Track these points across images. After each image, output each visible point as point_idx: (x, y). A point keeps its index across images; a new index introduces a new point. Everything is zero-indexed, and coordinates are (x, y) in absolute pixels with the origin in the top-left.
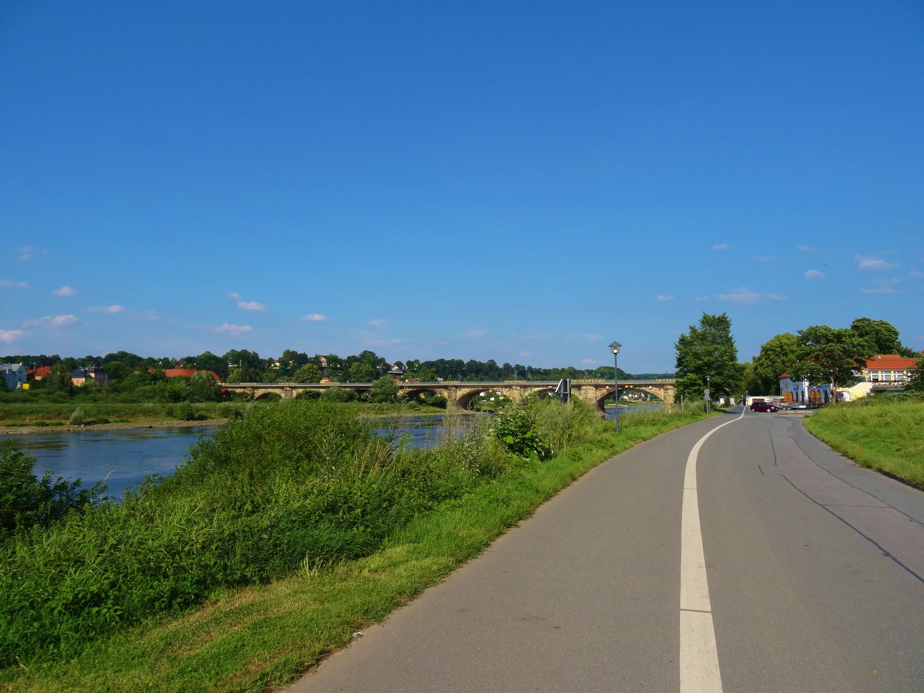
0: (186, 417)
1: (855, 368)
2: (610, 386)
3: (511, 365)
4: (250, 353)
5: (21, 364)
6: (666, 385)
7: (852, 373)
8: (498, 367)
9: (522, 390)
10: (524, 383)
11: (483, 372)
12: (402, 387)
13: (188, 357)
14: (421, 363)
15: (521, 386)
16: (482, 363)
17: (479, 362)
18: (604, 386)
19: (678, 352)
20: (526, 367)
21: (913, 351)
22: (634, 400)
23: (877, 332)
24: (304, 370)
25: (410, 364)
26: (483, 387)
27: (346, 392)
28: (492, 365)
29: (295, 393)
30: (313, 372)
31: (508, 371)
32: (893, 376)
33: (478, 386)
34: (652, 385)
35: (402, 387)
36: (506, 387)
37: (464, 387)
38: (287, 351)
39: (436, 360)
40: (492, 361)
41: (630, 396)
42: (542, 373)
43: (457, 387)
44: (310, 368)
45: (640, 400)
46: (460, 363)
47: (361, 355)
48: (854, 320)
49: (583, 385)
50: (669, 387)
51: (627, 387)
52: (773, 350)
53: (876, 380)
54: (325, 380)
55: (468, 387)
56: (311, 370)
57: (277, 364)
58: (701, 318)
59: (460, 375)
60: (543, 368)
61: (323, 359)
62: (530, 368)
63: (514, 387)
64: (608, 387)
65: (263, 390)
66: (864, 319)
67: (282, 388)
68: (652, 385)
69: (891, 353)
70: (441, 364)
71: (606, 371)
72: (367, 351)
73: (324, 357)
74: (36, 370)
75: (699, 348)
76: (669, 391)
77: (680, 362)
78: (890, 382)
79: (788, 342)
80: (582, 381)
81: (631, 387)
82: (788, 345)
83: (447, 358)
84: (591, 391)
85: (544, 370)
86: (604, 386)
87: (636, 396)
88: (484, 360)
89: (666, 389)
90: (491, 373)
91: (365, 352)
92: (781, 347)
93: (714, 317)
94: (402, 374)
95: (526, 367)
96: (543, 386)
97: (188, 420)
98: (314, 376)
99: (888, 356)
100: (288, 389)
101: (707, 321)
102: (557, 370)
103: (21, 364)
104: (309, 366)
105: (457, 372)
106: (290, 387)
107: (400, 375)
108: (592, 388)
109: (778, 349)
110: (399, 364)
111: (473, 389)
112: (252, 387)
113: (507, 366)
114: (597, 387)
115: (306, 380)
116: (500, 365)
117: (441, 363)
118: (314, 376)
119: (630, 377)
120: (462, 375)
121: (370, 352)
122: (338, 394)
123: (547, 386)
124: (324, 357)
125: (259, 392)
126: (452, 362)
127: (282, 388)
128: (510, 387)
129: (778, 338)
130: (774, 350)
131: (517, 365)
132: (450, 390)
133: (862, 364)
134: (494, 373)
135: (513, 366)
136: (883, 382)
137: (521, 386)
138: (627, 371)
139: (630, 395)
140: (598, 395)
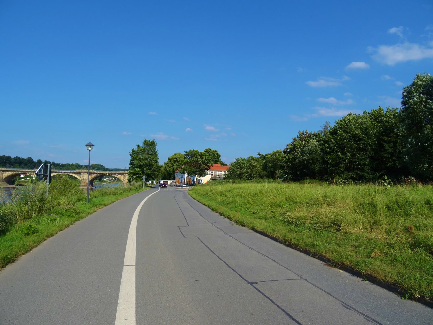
2: (96, 173)
6: (125, 174)
16: (23, 159)
17: (22, 158)
18: (93, 173)
19: (131, 157)
22: (109, 181)
23: (213, 154)
33: (18, 171)
37: (9, 171)
40: (30, 158)
42: (60, 166)
43: (3, 171)
45: (112, 181)
46: (9, 158)
49: (82, 173)
50: (126, 175)
51: (105, 174)
53: (212, 175)
55: (11, 171)
60: (61, 163)
64: (95, 174)
66: (209, 149)
69: (217, 164)
75: (141, 156)
76: (126, 177)
78: (217, 175)
79: (179, 156)
80: (81, 171)
81: (108, 174)
82: (179, 158)
84: (86, 176)
85: (62, 164)
86: (93, 173)
87: (110, 179)
89: (125, 176)
92: (177, 159)
96: (59, 172)
99: (216, 165)
105: (6, 163)
108: (87, 174)
109: (175, 160)
129: (175, 154)
130: (173, 160)
133: (209, 168)
134: (31, 164)
136: (214, 175)
138: (106, 167)
139: (107, 178)
140: (90, 178)
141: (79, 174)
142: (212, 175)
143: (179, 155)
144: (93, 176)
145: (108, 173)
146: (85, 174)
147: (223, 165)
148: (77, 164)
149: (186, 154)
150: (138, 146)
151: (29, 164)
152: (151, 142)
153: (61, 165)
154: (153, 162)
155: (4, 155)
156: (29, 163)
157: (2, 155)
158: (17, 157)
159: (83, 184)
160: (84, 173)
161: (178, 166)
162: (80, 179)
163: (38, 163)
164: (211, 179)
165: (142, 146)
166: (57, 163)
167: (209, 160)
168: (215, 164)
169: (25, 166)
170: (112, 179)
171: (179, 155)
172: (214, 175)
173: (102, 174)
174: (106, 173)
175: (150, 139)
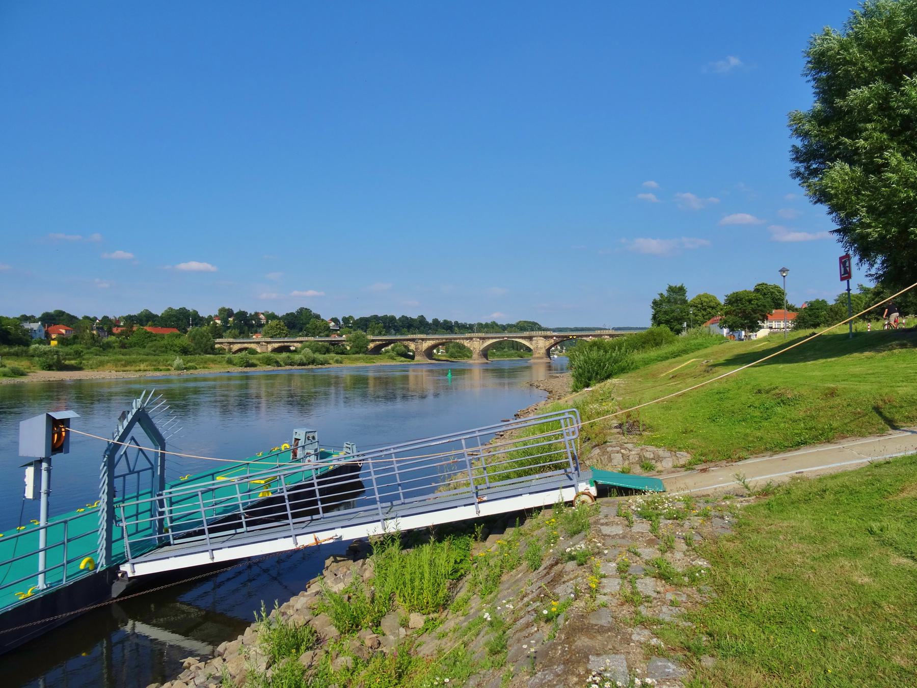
0: (245, 364)
1: (760, 320)
2: (557, 337)
5: (40, 323)
6: (604, 335)
7: (758, 323)
10: (482, 335)
12: (373, 341)
15: (480, 338)
16: (413, 319)
18: (552, 337)
19: (653, 311)
20: (453, 322)
21: (796, 307)
23: (772, 293)
25: (346, 320)
27: (323, 346)
28: (422, 320)
29: (270, 347)
30: (280, 328)
31: (437, 326)
32: (782, 325)
35: (373, 341)
36: (467, 339)
37: (429, 339)
39: (140, 312)
40: (422, 316)
42: (467, 328)
43: (423, 340)
44: (277, 325)
46: (392, 319)
47: (298, 312)
48: (756, 285)
49: (535, 337)
51: (571, 337)
52: (695, 306)
53: (771, 328)
55: (433, 339)
57: (218, 322)
58: (667, 288)
60: (468, 323)
61: (262, 316)
62: (456, 323)
64: (555, 338)
66: (763, 284)
67: (258, 343)
69: (781, 308)
71: (525, 325)
73: (263, 314)
74: (48, 328)
75: (665, 307)
77: (654, 318)
78: (780, 329)
79: (706, 300)
80: (533, 333)
81: (575, 337)
82: (707, 302)
84: (541, 341)
85: (469, 325)
86: (552, 337)
88: (415, 316)
91: (302, 309)
92: (702, 304)
93: (676, 287)
94: (338, 330)
95: (453, 322)
96: (499, 338)
97: (246, 367)
99: (779, 311)
100: (264, 344)
101: (671, 289)
102: (482, 324)
103: (40, 323)
105: (390, 327)
106: (265, 342)
107: (337, 330)
108: (542, 338)
109: (700, 306)
110: (335, 320)
111: (437, 341)
112: (228, 343)
114: (546, 337)
116: (430, 320)
117: (375, 318)
121: (306, 309)
122: (317, 348)
123: (503, 337)
124: (263, 314)
125: (236, 347)
126: (385, 317)
127: (258, 343)
128: (471, 339)
129: (699, 297)
130: (696, 306)
131: (445, 321)
133: (764, 318)
135: (442, 322)
136: (775, 329)
137: (480, 338)
138: (543, 325)
141: (530, 338)
142: (771, 328)
144: (552, 341)
146: (539, 338)
147: (793, 311)
148: (494, 322)
149: (726, 298)
150: (661, 295)
151: (422, 328)
152: (679, 287)
154: (684, 314)
155: (166, 308)
159: (537, 355)
160: (537, 336)
161: (705, 317)
162: (532, 347)
164: (770, 332)
165: (666, 294)
167: (765, 306)
168: (776, 309)
172: (775, 329)
173: (566, 337)
174: (573, 336)
175: (677, 284)
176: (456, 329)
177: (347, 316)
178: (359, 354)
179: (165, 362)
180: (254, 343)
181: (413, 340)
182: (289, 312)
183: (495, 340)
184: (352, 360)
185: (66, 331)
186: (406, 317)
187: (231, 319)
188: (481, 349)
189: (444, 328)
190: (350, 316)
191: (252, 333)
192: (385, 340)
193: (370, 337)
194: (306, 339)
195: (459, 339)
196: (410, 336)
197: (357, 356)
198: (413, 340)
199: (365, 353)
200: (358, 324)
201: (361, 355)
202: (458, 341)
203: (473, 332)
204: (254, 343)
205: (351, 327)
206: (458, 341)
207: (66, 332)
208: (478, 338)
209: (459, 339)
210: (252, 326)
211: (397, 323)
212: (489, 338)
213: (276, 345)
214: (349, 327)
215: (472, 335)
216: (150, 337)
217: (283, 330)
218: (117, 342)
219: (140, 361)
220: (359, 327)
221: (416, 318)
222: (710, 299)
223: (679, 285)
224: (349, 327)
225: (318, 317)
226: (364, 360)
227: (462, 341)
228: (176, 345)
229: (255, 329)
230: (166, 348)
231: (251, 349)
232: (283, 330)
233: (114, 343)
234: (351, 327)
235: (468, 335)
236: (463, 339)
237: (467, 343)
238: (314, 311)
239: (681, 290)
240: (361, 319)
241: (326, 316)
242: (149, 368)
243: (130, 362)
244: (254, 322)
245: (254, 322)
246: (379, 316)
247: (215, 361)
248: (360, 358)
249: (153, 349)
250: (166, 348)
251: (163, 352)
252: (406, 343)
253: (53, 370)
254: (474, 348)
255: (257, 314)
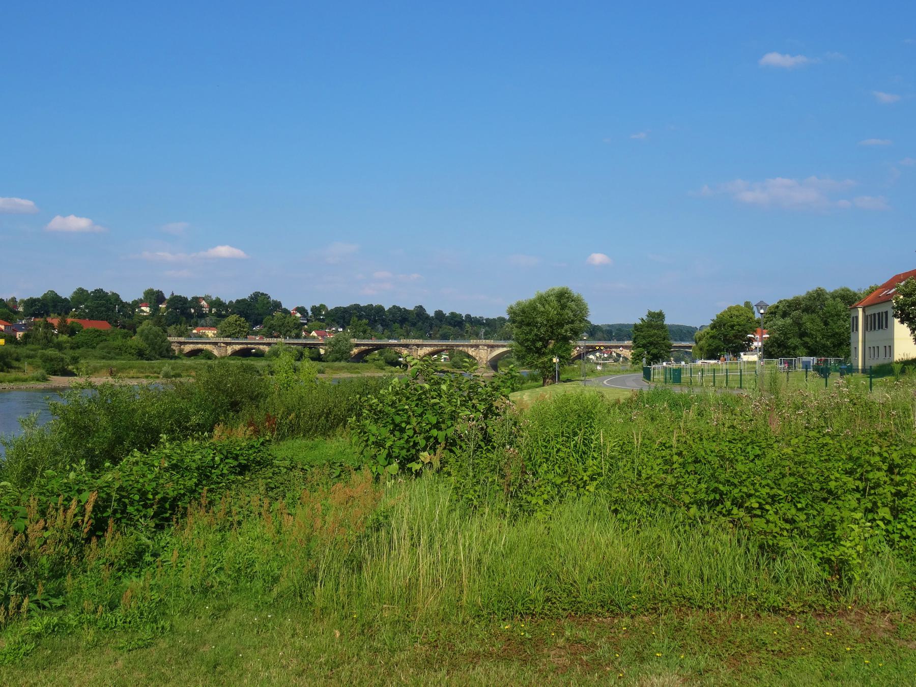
3: (444, 313)
4: (107, 293)
8: (428, 316)
9: (489, 350)
10: (491, 342)
11: (408, 321)
13: (31, 298)
14: (329, 309)
15: (489, 346)
16: (407, 310)
17: (404, 309)
24: (229, 323)
25: (317, 310)
26: (447, 346)
29: (230, 350)
30: (240, 324)
31: (441, 321)
33: (442, 345)
34: (622, 346)
35: (357, 345)
36: (472, 346)
37: (426, 346)
38: (149, 290)
40: (421, 307)
41: (598, 356)
42: (483, 324)
43: (418, 346)
44: (236, 321)
45: (611, 361)
46: (380, 309)
47: (251, 298)
51: (597, 348)
54: (213, 332)
55: (430, 346)
56: (238, 322)
58: (647, 313)
59: (379, 326)
60: (485, 317)
61: (204, 303)
62: (468, 316)
63: (481, 347)
65: (191, 345)
68: (622, 346)
70: (355, 311)
72: (259, 293)
79: (736, 313)
83: (363, 304)
85: (487, 320)
87: (606, 355)
90: (420, 323)
98: (242, 329)
100: (222, 345)
101: (651, 315)
104: (235, 318)
105: (376, 321)
106: (224, 343)
110: (301, 310)
113: (439, 314)
115: (233, 334)
116: (431, 312)
117: (355, 309)
118: (242, 329)
119: (598, 329)
120: (382, 326)
121: (262, 294)
124: (204, 299)
126: (370, 308)
128: (477, 346)
129: (730, 309)
131: (452, 313)
132: (411, 349)
134: (423, 323)
135: (448, 315)
137: (489, 346)
143: (738, 311)
145: (603, 346)
153: (484, 321)
156: (419, 321)
157: (366, 305)
158: (394, 306)
163: (436, 318)
165: (645, 318)
166: (476, 317)
169: (412, 328)
170: (610, 356)
171: (738, 311)
176: (468, 325)
177: (317, 305)
178: (340, 361)
179: (151, 369)
180: (209, 343)
181: (406, 346)
182: (240, 298)
183: (505, 349)
184: (335, 370)
185: (6, 326)
186: (399, 308)
187: (162, 306)
188: (489, 358)
189: (450, 324)
190: (321, 305)
191: (190, 326)
192: (371, 345)
193: (355, 341)
194: (275, 340)
195: (463, 346)
196: (403, 341)
197: (337, 364)
198: (406, 346)
199: (347, 360)
200: (332, 316)
201: (343, 364)
202: (461, 348)
203: (480, 339)
204: (209, 343)
205: (323, 320)
206: (461, 348)
207: (5, 328)
208: (485, 345)
209: (463, 346)
210: (191, 316)
211: (386, 315)
212: (498, 346)
213: (237, 347)
214: (319, 320)
215: (478, 342)
216: (99, 336)
217: (243, 327)
218: (68, 342)
219: (129, 368)
220: (334, 320)
221: (412, 309)
222: (741, 312)
223: (657, 311)
224: (319, 320)
225: (277, 305)
226: (349, 370)
227: (465, 349)
228: (131, 347)
229: (195, 320)
230: (120, 349)
231: (207, 351)
232: (243, 327)
233: (65, 343)
234: (323, 320)
235: (473, 342)
236: (467, 346)
237: (471, 352)
238: (274, 297)
239: (660, 316)
240: (337, 310)
241: (289, 305)
242: (138, 375)
243: (122, 369)
244: (193, 311)
245: (193, 311)
246: (362, 305)
247: (196, 368)
248: (343, 367)
249: (105, 350)
250: (120, 349)
251: (118, 354)
252: (398, 349)
253: (58, 375)
254: (480, 358)
255: (196, 300)
